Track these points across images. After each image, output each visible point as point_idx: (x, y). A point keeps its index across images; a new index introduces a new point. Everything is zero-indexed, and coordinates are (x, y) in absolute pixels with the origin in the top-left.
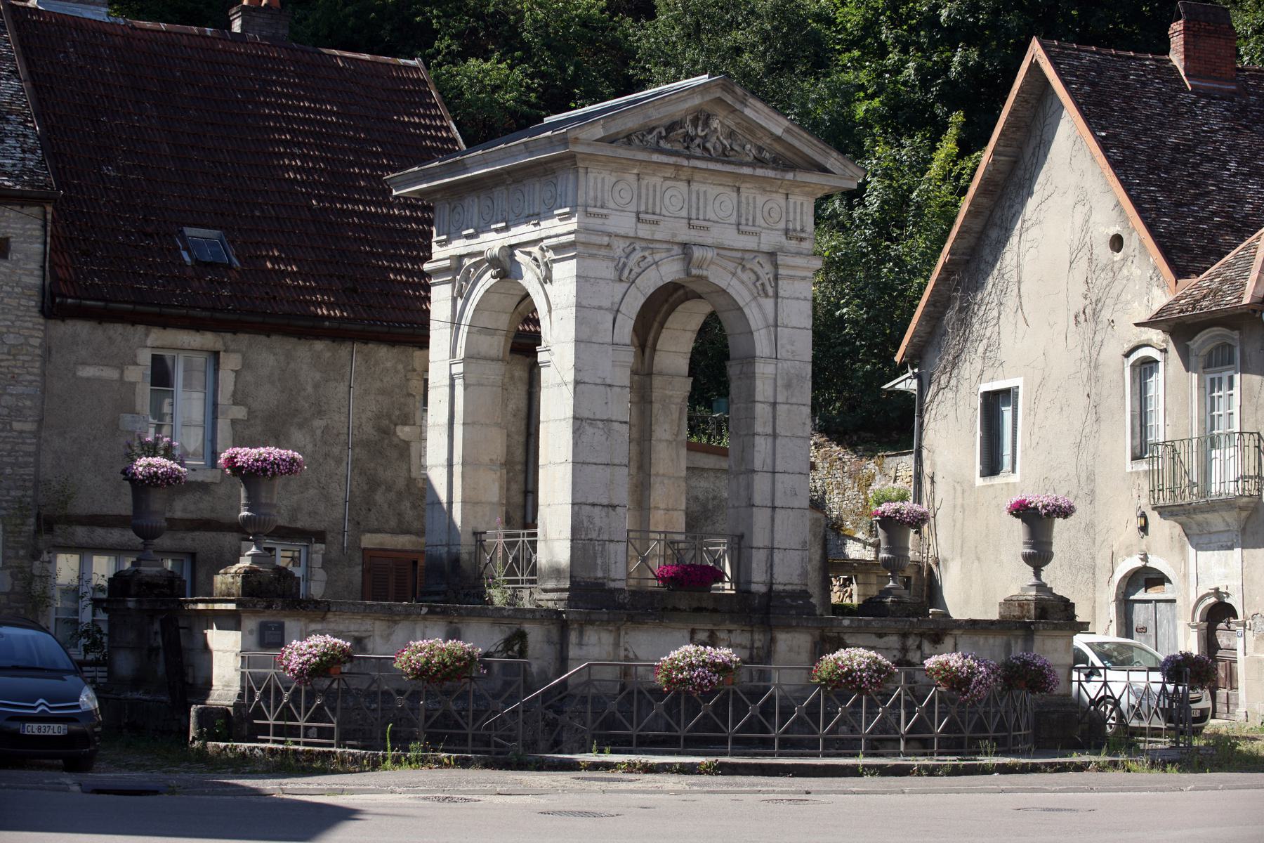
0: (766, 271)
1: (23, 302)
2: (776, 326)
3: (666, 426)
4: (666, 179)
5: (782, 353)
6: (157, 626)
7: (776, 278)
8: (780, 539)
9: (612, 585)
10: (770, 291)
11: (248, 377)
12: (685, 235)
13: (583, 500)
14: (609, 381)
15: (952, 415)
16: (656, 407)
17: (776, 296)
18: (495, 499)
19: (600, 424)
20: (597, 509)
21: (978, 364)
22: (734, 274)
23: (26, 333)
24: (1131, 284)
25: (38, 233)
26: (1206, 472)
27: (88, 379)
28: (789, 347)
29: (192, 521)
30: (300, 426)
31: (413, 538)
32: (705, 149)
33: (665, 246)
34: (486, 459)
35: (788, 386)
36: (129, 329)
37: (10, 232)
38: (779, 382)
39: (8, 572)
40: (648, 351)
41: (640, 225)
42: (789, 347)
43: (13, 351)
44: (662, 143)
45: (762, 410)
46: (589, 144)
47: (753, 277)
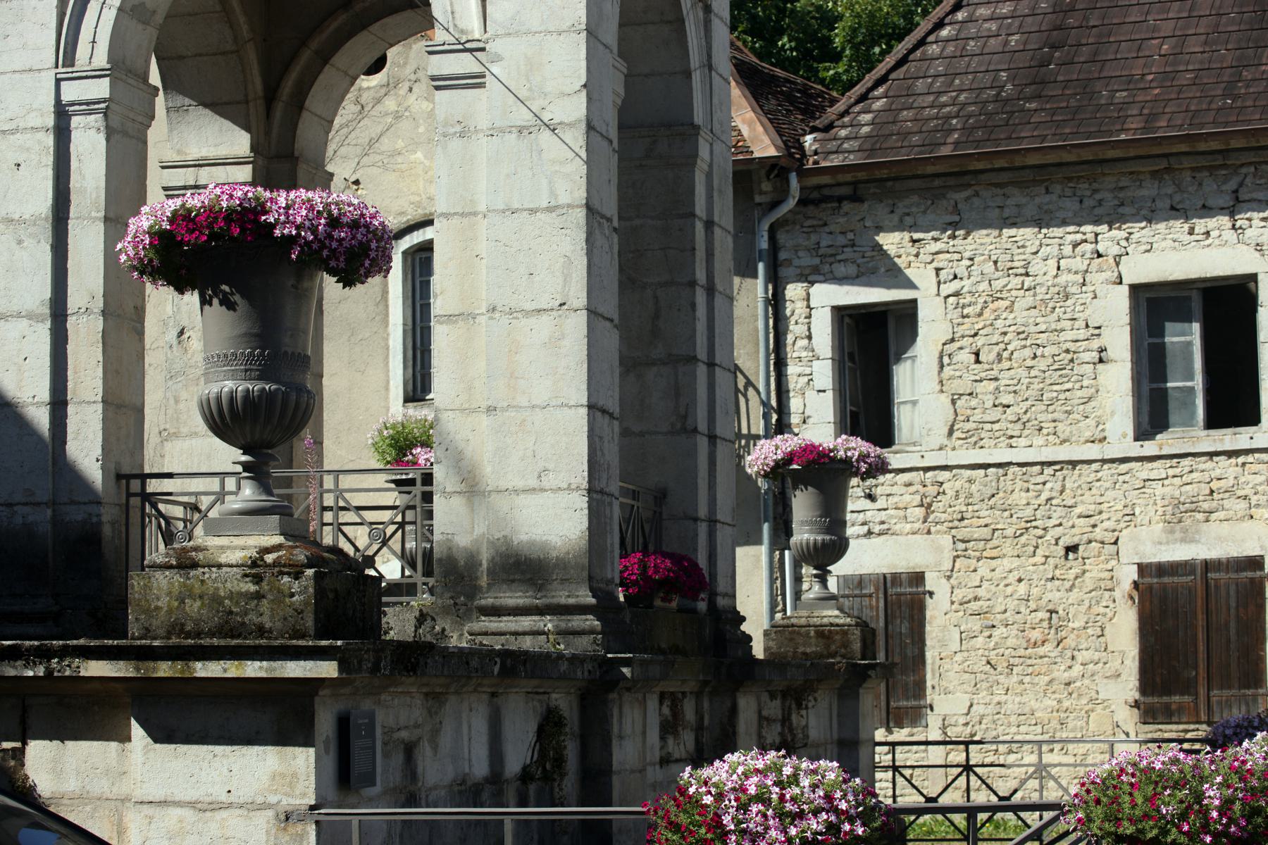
24: (405, 125)
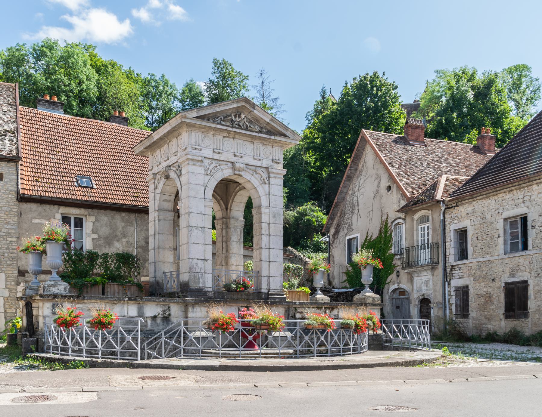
0: (265, 176)
1: (10, 196)
2: (269, 195)
3: (236, 236)
4: (224, 137)
5: (271, 205)
7: (269, 177)
8: (272, 273)
9: (206, 289)
10: (267, 182)
11: (98, 224)
12: (232, 159)
13: (193, 257)
14: (203, 213)
15: (339, 246)
16: (232, 229)
17: (269, 184)
18: (172, 261)
19: (200, 229)
20: (199, 261)
21: (346, 231)
22: (252, 175)
23: (12, 207)
25: (14, 172)
26: (418, 257)
27: (36, 223)
28: (274, 203)
30: (118, 241)
32: (239, 125)
33: (225, 163)
34: (168, 247)
35: (274, 217)
37: (3, 171)
38: (271, 216)
39: (8, 290)
40: (228, 210)
41: (214, 154)
42: (274, 203)
43: (6, 213)
44: (222, 122)
45: (264, 226)
46: (191, 119)
47: (260, 176)
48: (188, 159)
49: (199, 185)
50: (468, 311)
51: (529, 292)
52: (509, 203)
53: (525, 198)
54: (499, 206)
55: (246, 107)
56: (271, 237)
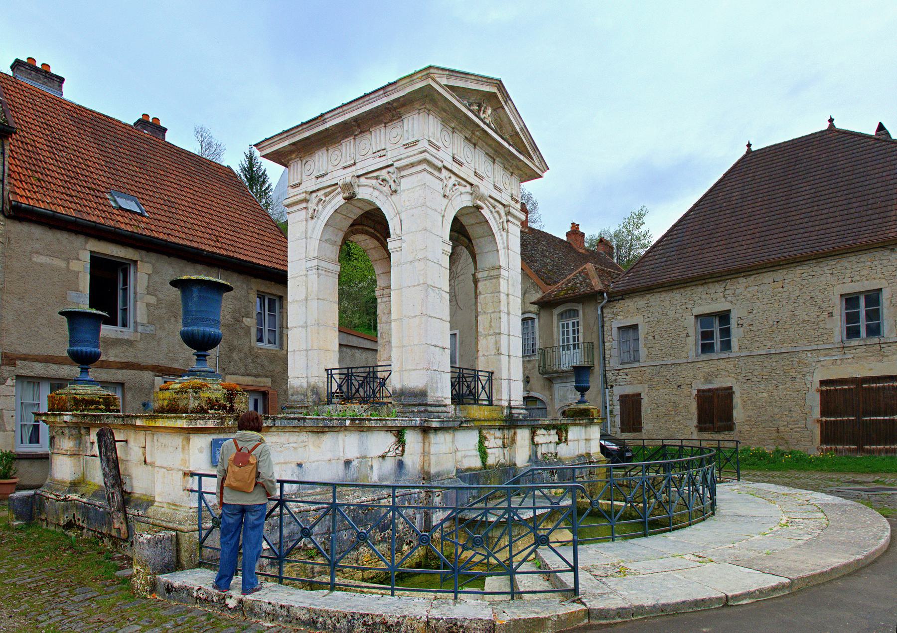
6: (93, 437)
11: (156, 278)
27: (41, 265)
29: (121, 363)
31: (253, 378)
36: (73, 238)
48: (426, 161)
49: (436, 210)
50: (640, 423)
51: (735, 401)
52: (703, 296)
53: (727, 292)
54: (687, 301)
55: (497, 97)
56: (309, 329)
